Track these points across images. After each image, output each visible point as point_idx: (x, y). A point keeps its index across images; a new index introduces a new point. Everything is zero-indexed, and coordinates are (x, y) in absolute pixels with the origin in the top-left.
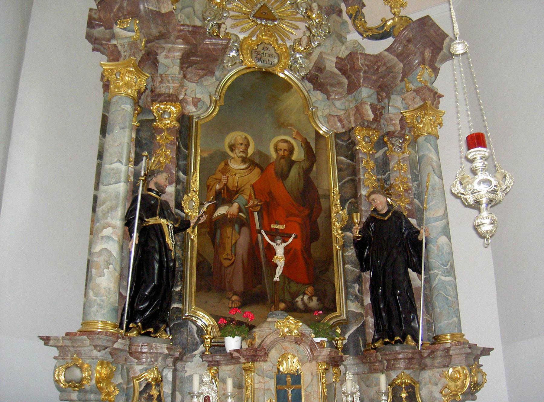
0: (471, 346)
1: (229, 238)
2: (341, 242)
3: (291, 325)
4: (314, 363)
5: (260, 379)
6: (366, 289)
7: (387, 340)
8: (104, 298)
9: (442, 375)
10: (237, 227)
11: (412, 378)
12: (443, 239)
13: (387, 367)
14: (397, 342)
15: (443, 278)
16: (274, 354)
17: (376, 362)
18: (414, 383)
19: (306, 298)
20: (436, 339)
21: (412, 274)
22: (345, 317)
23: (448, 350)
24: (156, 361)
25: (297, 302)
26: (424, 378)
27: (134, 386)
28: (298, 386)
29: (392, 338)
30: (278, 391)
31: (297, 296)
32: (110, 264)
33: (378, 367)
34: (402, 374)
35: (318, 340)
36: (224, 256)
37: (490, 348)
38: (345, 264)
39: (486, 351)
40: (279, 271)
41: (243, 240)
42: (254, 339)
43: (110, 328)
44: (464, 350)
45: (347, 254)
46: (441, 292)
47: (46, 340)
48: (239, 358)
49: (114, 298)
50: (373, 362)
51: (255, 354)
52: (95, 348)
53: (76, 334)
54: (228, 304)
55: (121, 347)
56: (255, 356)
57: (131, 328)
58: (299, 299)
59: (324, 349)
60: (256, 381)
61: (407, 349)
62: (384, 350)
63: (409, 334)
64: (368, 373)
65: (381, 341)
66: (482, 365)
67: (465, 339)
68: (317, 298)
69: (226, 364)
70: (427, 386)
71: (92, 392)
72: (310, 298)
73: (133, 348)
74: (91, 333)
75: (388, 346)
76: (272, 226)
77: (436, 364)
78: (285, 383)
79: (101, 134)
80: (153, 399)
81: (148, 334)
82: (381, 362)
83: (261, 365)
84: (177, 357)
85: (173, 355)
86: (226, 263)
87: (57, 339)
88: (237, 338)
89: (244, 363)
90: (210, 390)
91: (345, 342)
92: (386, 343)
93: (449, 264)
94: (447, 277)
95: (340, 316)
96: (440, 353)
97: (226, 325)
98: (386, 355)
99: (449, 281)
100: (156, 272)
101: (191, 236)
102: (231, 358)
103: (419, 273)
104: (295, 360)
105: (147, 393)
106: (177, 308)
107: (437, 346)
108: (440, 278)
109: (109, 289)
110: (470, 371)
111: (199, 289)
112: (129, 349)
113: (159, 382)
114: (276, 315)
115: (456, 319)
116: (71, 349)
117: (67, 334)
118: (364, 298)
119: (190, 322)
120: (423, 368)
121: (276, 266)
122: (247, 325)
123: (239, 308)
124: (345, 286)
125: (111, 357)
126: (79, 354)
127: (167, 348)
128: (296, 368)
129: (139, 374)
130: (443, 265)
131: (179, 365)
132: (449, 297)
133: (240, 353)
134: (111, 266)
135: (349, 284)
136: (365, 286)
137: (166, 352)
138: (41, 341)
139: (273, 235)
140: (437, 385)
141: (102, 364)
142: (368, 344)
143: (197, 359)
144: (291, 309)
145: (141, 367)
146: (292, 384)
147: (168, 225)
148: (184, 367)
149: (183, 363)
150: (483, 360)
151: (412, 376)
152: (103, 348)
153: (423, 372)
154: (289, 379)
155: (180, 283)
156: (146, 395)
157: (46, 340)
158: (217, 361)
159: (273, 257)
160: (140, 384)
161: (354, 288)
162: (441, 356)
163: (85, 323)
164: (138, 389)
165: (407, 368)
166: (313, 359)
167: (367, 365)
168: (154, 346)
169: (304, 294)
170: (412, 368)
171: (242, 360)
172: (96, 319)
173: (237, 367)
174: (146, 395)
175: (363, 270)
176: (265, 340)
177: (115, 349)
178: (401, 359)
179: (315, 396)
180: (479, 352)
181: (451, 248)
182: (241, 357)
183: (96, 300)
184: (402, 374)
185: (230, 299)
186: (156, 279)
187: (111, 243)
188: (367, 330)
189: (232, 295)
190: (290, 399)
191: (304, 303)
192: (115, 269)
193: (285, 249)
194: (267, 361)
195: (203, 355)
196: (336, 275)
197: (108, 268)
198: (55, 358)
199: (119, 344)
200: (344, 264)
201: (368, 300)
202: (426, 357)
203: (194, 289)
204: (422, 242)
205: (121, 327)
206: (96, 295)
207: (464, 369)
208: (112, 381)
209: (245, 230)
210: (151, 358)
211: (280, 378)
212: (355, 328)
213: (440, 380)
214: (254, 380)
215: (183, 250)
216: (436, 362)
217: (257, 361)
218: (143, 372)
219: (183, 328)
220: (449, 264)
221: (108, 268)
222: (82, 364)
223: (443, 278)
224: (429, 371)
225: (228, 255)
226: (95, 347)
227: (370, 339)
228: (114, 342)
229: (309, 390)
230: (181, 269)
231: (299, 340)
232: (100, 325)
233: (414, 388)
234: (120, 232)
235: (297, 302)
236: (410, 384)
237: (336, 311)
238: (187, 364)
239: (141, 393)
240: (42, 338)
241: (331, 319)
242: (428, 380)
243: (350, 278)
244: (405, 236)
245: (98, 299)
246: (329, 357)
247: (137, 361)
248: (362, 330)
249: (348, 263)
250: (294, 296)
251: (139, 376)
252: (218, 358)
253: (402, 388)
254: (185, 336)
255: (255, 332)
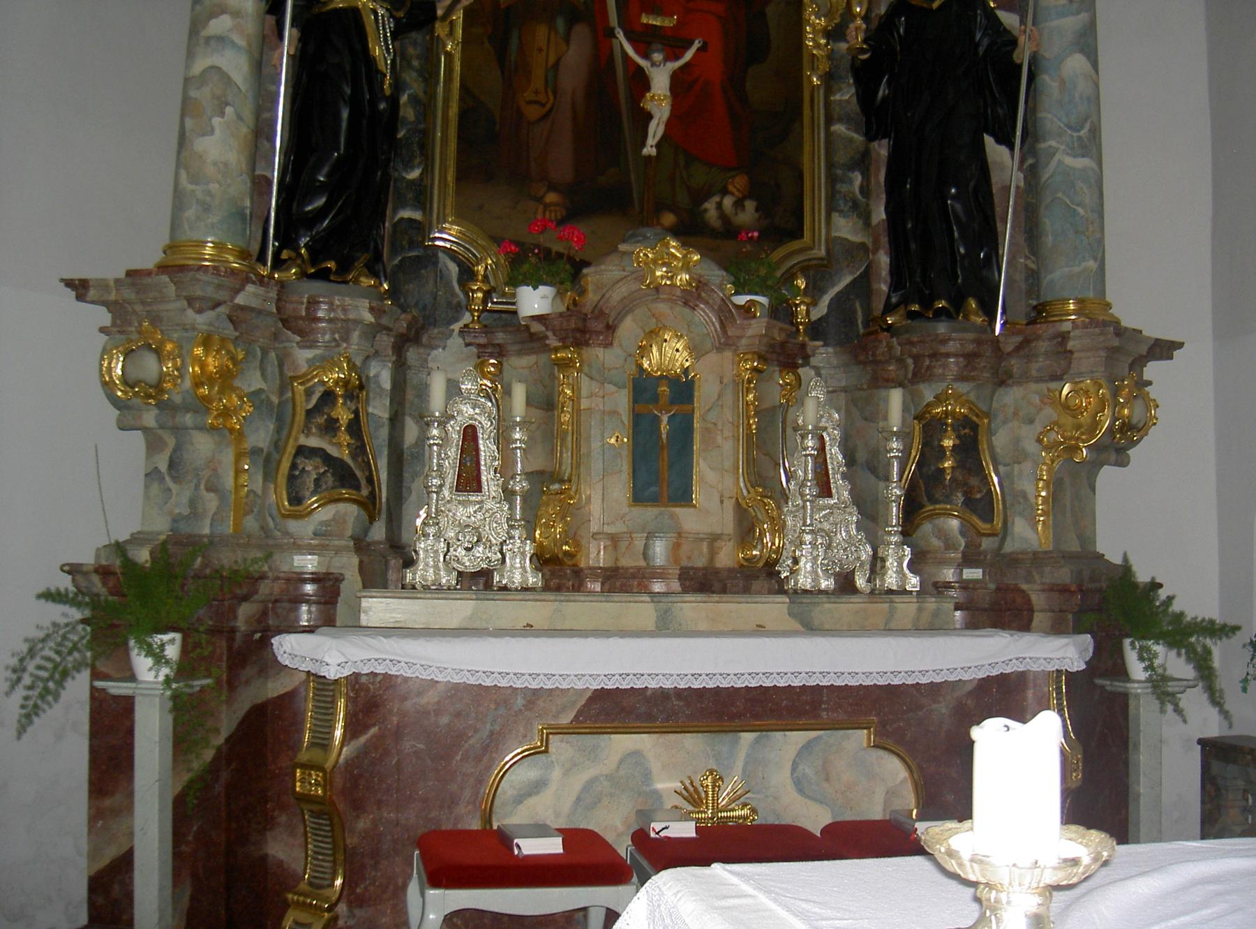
0: (1120, 331)
1: (540, 50)
2: (824, 66)
3: (671, 263)
4: (728, 354)
5: (595, 387)
6: (878, 182)
7: (915, 308)
8: (214, 187)
9: (1053, 399)
10: (560, 23)
11: (972, 403)
12: (1076, 63)
13: (914, 374)
14: (939, 313)
15: (1069, 160)
16: (628, 329)
17: (887, 362)
18: (977, 416)
19: (728, 202)
20: (1041, 312)
21: (994, 150)
22: (823, 253)
23: (1064, 337)
24: (346, 339)
25: (706, 211)
26: (1005, 405)
27: (293, 399)
28: (686, 407)
29: (927, 303)
30: (637, 418)
31: (706, 198)
32: (227, 104)
33: (893, 375)
34: (949, 393)
35: (741, 300)
36: (529, 95)
37: (1173, 342)
38: (831, 124)
39: (1164, 349)
40: (656, 130)
41: (575, 55)
42: (583, 292)
43: (231, 259)
44: (1102, 339)
45: (838, 97)
46: (1060, 195)
47: (80, 288)
48: (546, 337)
49: (240, 187)
50: (880, 362)
51: (582, 328)
52: (190, 305)
53: (148, 273)
54: (536, 213)
55: (255, 303)
56: (583, 331)
57: (285, 261)
58: (710, 206)
59: (753, 322)
60: (584, 392)
61: (964, 330)
62: (907, 332)
63: (975, 296)
64: (869, 388)
65: (902, 311)
66: (1149, 383)
67: (1112, 315)
68: (755, 204)
69: (520, 353)
70: (1010, 425)
71: (187, 409)
72: (739, 204)
73: (289, 308)
74: (183, 268)
75: (916, 323)
76: (644, 20)
77: (1034, 373)
78: (655, 399)
79: (601, 696)
80: (339, 428)
81: (323, 275)
82: (901, 361)
83: (598, 354)
84: (403, 335)
85: (388, 329)
86: (533, 112)
87: (103, 285)
88: (543, 290)
89: (556, 350)
90: (477, 411)
91: (816, 314)
92: (912, 315)
93: (1088, 126)
94: (1080, 160)
95: (812, 249)
96: (1043, 346)
97: (526, 264)
98: (912, 343)
99: (1084, 169)
100: (344, 125)
101: (445, 46)
102: (530, 336)
103: (1011, 147)
104: (680, 346)
105: (323, 414)
106: (410, 220)
107: (1040, 329)
108: (1062, 159)
109: (226, 165)
110: (1116, 393)
111: (461, 176)
112: (278, 309)
113: (356, 390)
114: (645, 237)
115: (1092, 264)
116: (138, 308)
117: (129, 273)
118: (873, 207)
119: (441, 255)
120: (1003, 380)
121: (649, 117)
122: (571, 259)
123: (561, 222)
124: (827, 177)
125: (231, 327)
126: (155, 320)
127: (372, 309)
128: (682, 365)
129: (304, 368)
130: (1070, 127)
131: (412, 354)
132: (1080, 210)
133: (545, 325)
134: (229, 110)
135: (839, 172)
136: (877, 175)
137: (369, 317)
138: (69, 290)
139: (645, 40)
140: (1031, 421)
141: (206, 343)
142: (874, 320)
143: (456, 342)
144: (690, 230)
145: (309, 354)
146: (673, 402)
147: (375, 12)
148: (426, 361)
149: (422, 350)
150: (1152, 370)
151: (972, 397)
152: (210, 304)
153: (1001, 390)
154: (664, 389)
155: (417, 160)
156: (321, 420)
157: (80, 288)
158: (499, 345)
159: (643, 96)
160: (309, 393)
161: (851, 182)
162: (1046, 353)
163: (171, 248)
164: (303, 405)
165: (961, 378)
166: (726, 343)
167: (869, 368)
168: (337, 302)
169: (724, 192)
170: (973, 379)
171: (553, 342)
172: (196, 236)
173: (543, 359)
174: (321, 420)
175: (871, 136)
176: (607, 296)
177: (242, 308)
178: (948, 355)
179: (727, 433)
180: (1143, 350)
181: (1097, 85)
182: (550, 334)
183: (193, 191)
184: (949, 393)
185: (540, 200)
186: (342, 140)
187: (229, 53)
188: (875, 286)
189: (543, 190)
190: (664, 436)
191: (722, 216)
192: (239, 117)
193: (676, 78)
194: (611, 344)
195: (465, 331)
196: (807, 148)
197: (222, 114)
198: (103, 330)
199: (249, 296)
200: (829, 121)
201: (879, 214)
202: (1009, 354)
203: (451, 177)
204: (1020, 67)
205: (261, 258)
206: (194, 179)
207: (1100, 387)
208: (237, 383)
209: (581, 32)
210: (333, 333)
211: (644, 388)
212: (847, 280)
213: (1041, 409)
214: (579, 389)
215: (425, 80)
216: (1034, 368)
217: (587, 345)
218: (317, 364)
219: (426, 267)
220: (1088, 126)
221: (222, 114)
222: (161, 344)
223: (1069, 160)
224: (1015, 388)
225: (536, 92)
226: (190, 301)
227: (878, 306)
228: (237, 291)
229: (712, 416)
230: (422, 126)
231: (693, 296)
232: (209, 250)
233: (975, 427)
234: (251, 26)
235: (706, 211)
236: (965, 416)
237: (802, 236)
238: (435, 352)
239: (309, 413)
240: (69, 283)
241: (784, 255)
242: (1012, 410)
243: (841, 157)
244: (981, 50)
245: (199, 190)
246: (765, 340)
247: (299, 338)
248: (862, 285)
249: (840, 120)
250: (699, 197)
251: (305, 375)
252: (500, 337)
253: (946, 424)
254: (430, 286)
255: (586, 275)
